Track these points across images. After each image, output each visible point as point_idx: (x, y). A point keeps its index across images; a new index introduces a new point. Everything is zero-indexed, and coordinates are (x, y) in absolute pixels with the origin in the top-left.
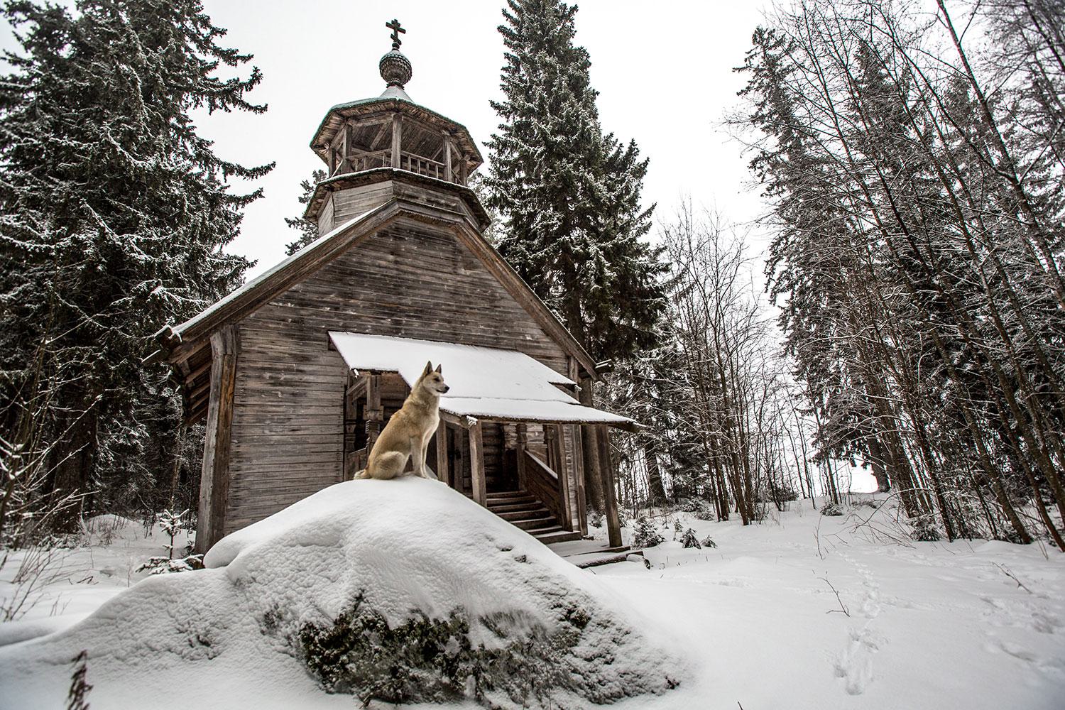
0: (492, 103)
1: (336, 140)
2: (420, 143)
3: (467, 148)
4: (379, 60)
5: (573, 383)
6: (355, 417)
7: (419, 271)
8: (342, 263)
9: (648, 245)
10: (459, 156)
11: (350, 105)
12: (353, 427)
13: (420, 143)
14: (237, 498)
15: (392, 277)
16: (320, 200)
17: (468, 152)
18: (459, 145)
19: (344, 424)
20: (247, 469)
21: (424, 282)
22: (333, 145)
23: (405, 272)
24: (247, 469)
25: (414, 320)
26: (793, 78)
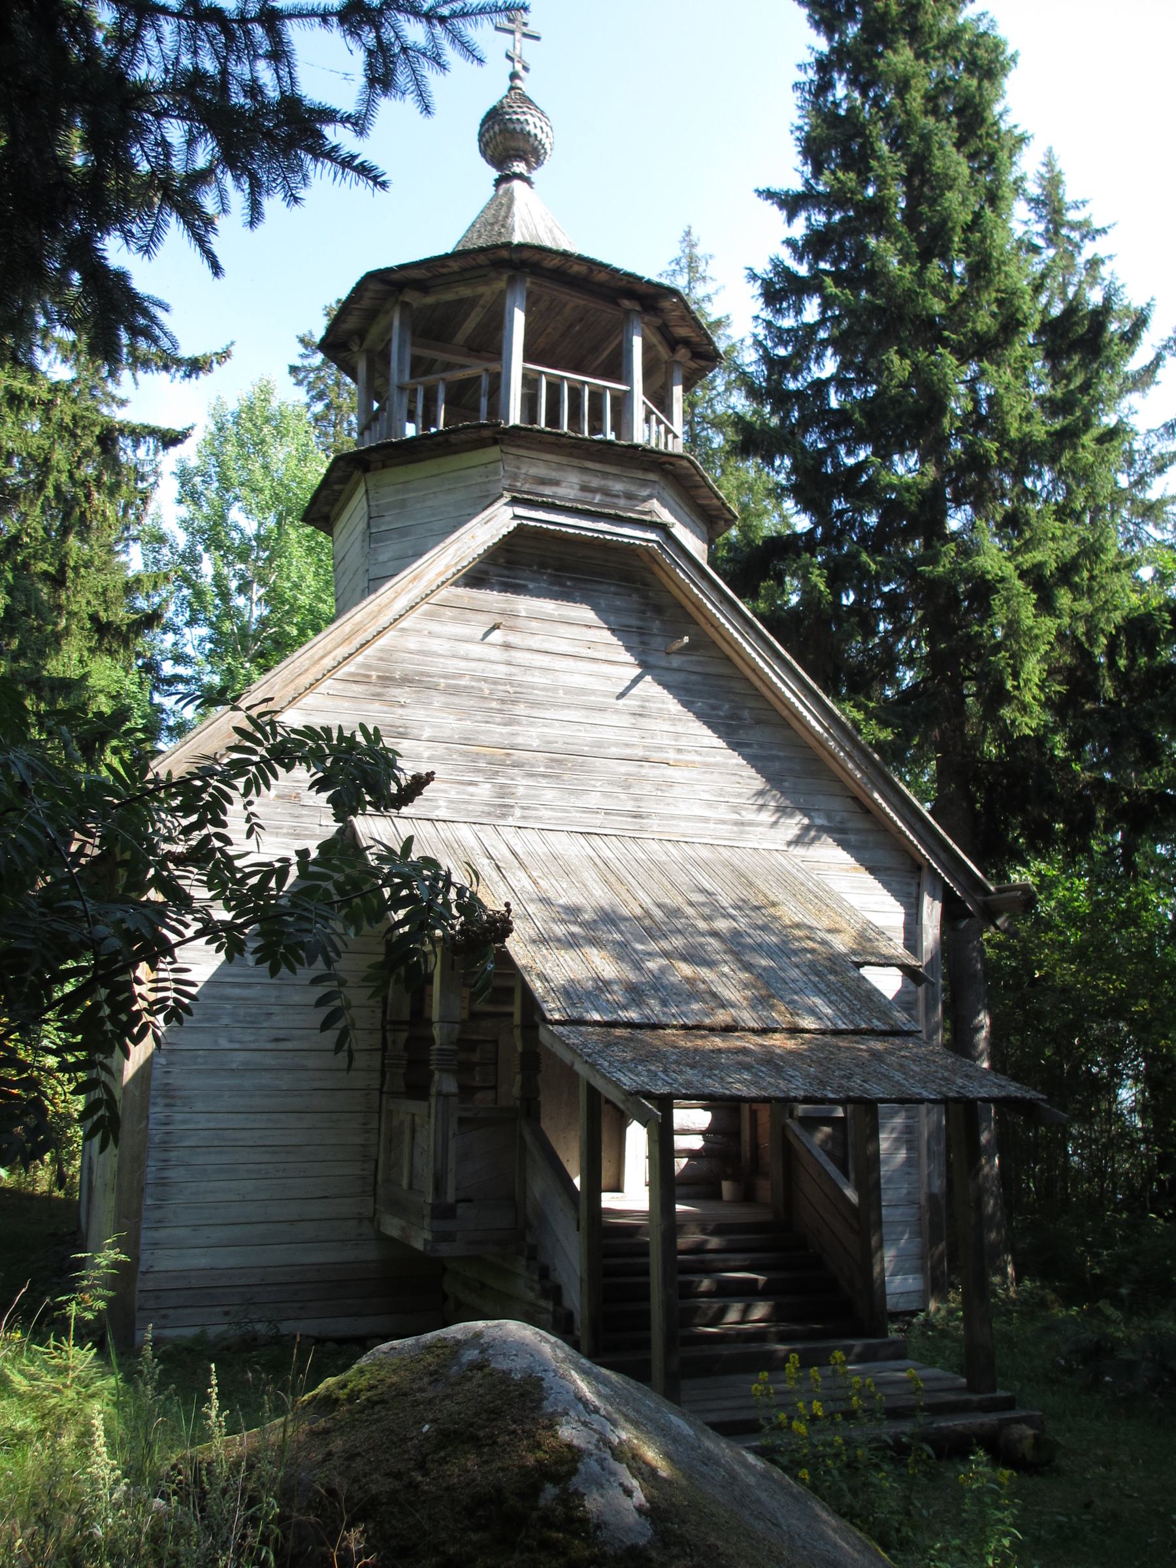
0: (427, 109)
1: (374, 332)
2: (571, 326)
3: (682, 332)
4: (482, 114)
5: (1031, 1094)
6: (406, 1015)
7: (559, 663)
8: (386, 656)
9: (755, 336)
10: (663, 351)
11: (498, 400)
12: (403, 1036)
13: (571, 326)
14: (163, 1183)
15: (495, 682)
16: (337, 487)
17: (686, 342)
18: (664, 331)
19: (383, 1028)
20: (184, 1122)
21: (568, 691)
22: (368, 343)
23: (528, 668)
24: (184, 1122)
25: (544, 782)
26: (153, 70)
